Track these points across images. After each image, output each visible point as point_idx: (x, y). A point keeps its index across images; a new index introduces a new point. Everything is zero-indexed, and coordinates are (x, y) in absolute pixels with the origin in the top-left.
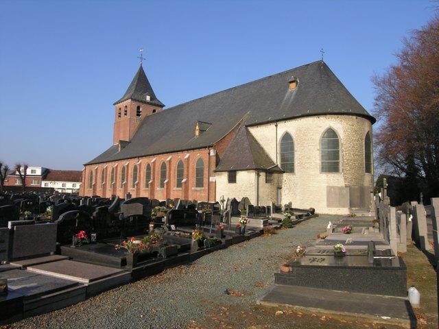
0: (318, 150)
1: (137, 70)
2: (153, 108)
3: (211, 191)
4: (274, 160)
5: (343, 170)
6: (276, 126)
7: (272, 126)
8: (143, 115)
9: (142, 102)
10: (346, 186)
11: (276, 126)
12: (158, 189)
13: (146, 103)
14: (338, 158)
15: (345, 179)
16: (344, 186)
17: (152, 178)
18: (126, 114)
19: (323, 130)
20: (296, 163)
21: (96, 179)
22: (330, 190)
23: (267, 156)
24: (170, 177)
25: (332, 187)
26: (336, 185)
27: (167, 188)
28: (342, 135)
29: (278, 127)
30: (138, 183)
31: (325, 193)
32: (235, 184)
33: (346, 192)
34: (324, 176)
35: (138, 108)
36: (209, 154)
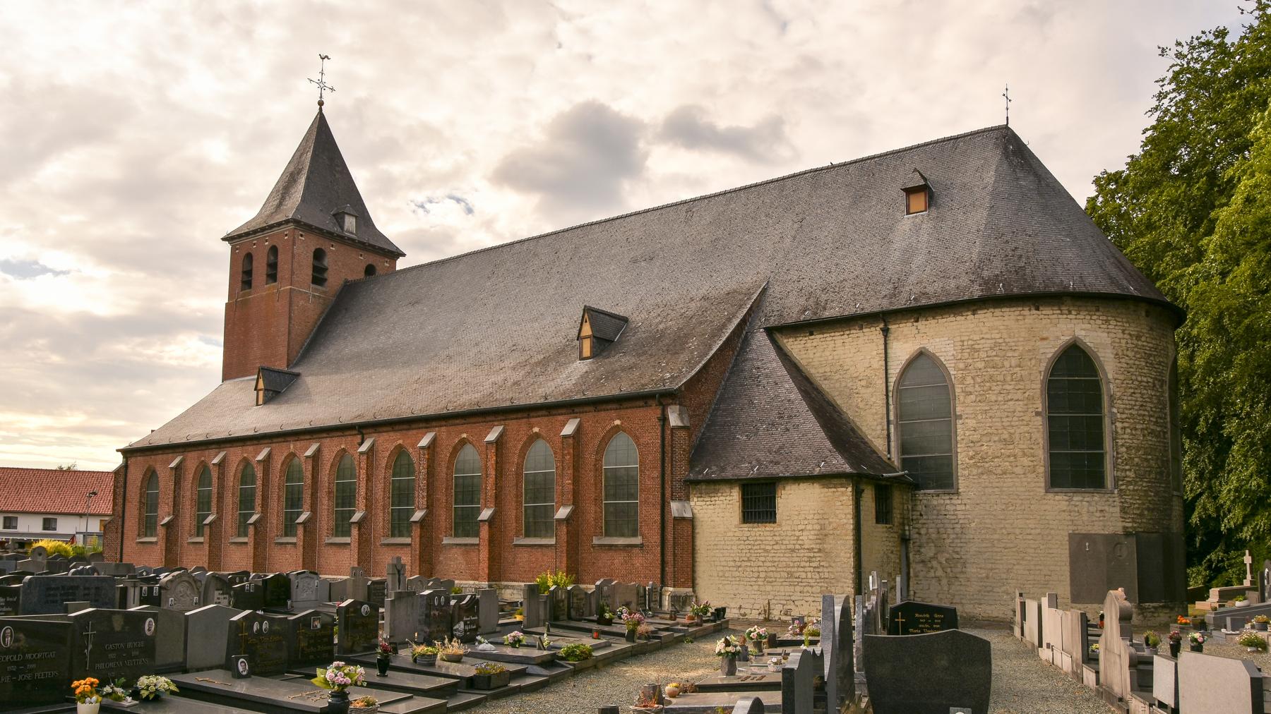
0: (1038, 414)
1: (306, 122)
2: (364, 259)
3: (128, 505)
4: (879, 444)
5: (1116, 480)
6: (886, 332)
7: (873, 334)
8: (335, 279)
9: (330, 236)
10: (1127, 534)
11: (886, 332)
12: (446, 541)
13: (342, 239)
14: (1099, 443)
15: (1123, 510)
16: (1120, 532)
17: (214, 509)
18: (272, 277)
19: (1050, 350)
20: (963, 457)
21: (176, 504)
22: (1080, 544)
23: (853, 430)
24: (265, 505)
25: (1087, 537)
26: (1097, 529)
27: (492, 541)
28: (1110, 366)
29: (891, 337)
30: (363, 519)
31: (1063, 554)
32: (769, 527)
33: (1128, 551)
34: (1060, 502)
35: (319, 255)
36: (664, 419)
